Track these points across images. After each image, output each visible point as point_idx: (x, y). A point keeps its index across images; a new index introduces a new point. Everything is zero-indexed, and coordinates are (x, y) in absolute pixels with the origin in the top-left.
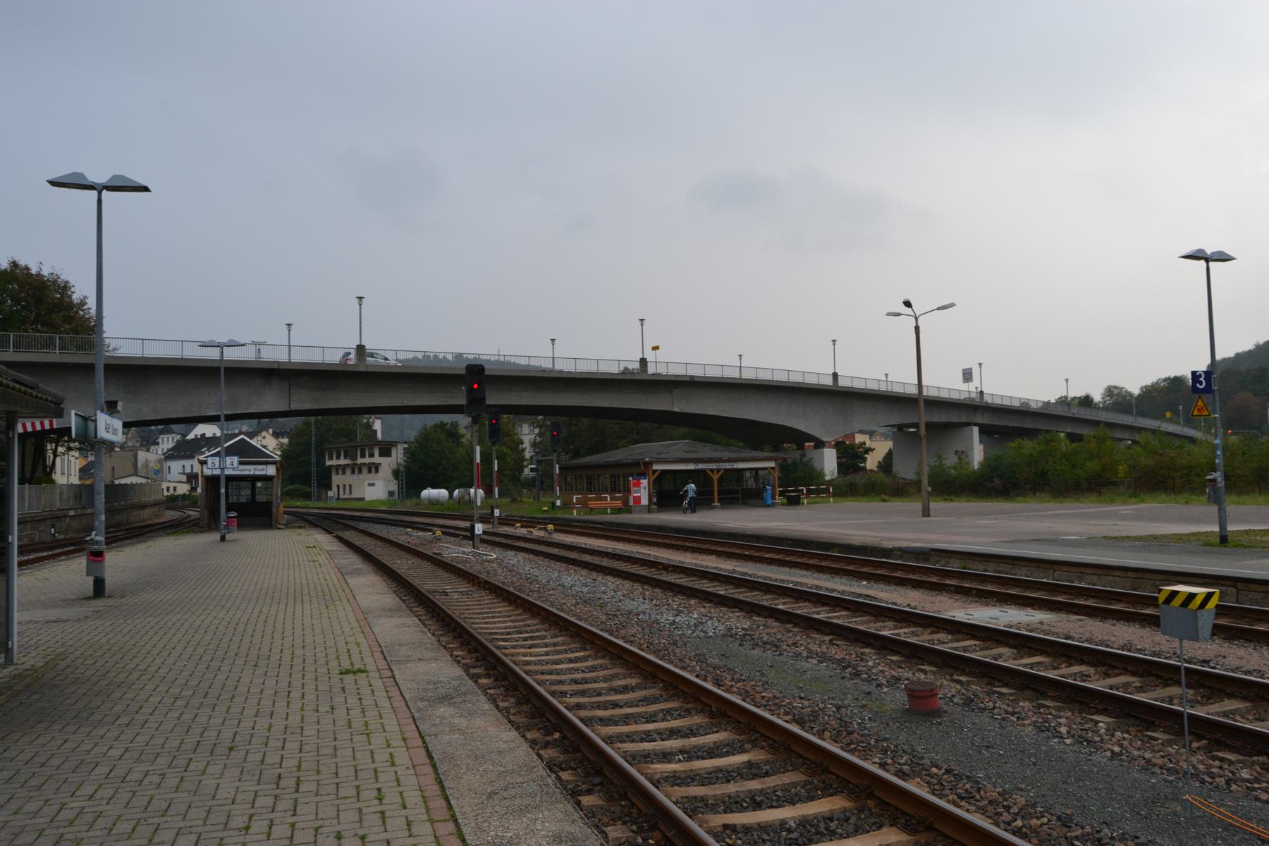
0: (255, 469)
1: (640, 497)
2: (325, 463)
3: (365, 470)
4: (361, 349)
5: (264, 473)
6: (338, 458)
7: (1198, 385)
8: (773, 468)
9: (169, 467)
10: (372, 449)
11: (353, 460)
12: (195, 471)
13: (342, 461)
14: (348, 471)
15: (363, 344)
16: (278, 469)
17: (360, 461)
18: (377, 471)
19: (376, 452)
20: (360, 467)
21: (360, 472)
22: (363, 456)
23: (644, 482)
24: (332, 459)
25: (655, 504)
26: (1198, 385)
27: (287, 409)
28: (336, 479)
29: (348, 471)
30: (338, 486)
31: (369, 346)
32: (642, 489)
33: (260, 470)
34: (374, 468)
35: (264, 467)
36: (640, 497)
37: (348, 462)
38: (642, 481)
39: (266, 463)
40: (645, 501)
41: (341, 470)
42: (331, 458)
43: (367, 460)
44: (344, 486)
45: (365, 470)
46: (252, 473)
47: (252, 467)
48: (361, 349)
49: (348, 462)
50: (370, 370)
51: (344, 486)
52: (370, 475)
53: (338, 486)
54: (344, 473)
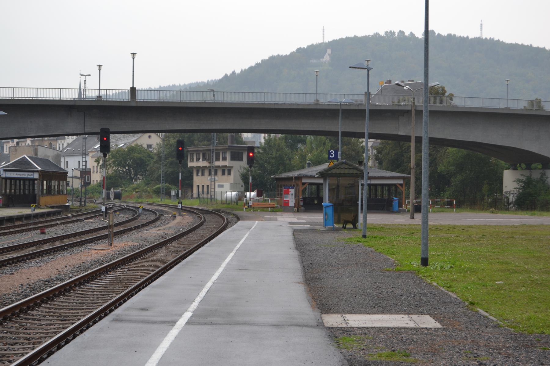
0: (28, 175)
1: (288, 201)
2: (187, 165)
3: (220, 172)
4: (133, 90)
5: (32, 177)
6: (198, 160)
7: (330, 156)
8: (401, 185)
9: (67, 162)
10: (225, 153)
11: (210, 163)
12: (88, 167)
13: (202, 163)
14: (207, 173)
15: (135, 87)
16: (40, 175)
17: (217, 163)
18: (229, 174)
19: (228, 156)
20: (216, 169)
21: (216, 174)
22: (218, 159)
23: (292, 191)
24: (193, 161)
25: (302, 206)
26: (330, 156)
27: (83, 132)
28: (198, 180)
29: (207, 173)
30: (198, 186)
31: (138, 86)
32: (290, 196)
33: (30, 175)
34: (226, 170)
35: (32, 173)
36: (288, 201)
37: (206, 164)
38: (290, 190)
39: (33, 171)
40: (292, 204)
41: (201, 170)
42: (192, 160)
43: (220, 163)
44: (203, 186)
45: (220, 172)
46: (26, 177)
47: (26, 173)
48: (133, 90)
49: (206, 164)
50: (139, 105)
51: (203, 186)
52: (224, 177)
53: (198, 186)
54: (203, 174)
